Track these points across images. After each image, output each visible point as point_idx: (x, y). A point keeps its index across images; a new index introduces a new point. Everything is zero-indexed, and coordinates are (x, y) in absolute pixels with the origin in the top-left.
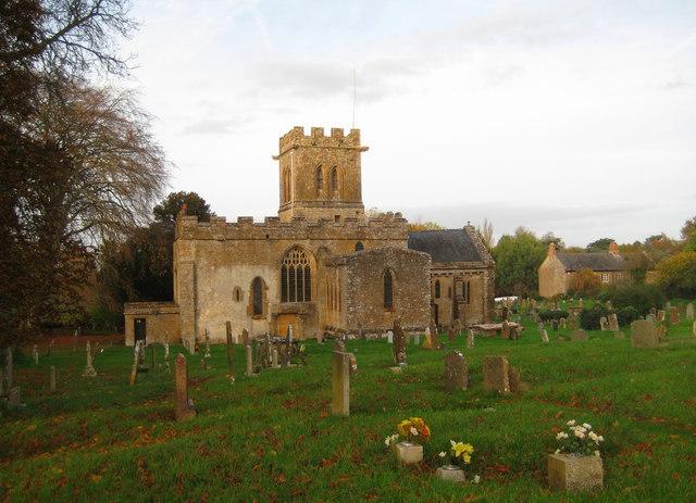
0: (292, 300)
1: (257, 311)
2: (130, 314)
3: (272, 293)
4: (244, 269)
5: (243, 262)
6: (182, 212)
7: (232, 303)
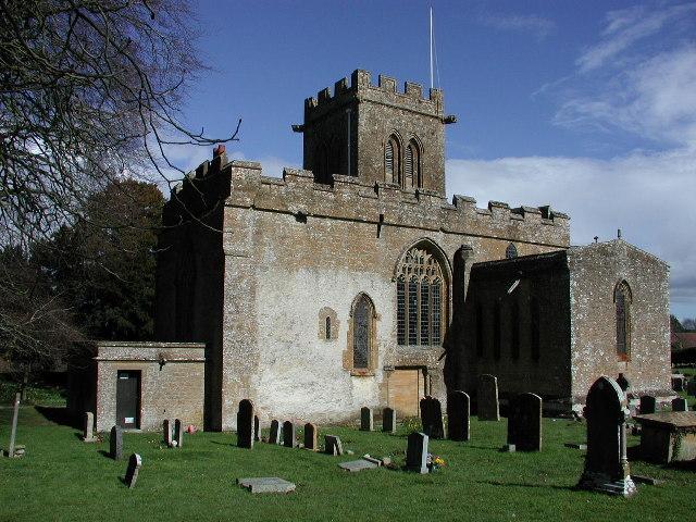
0: (413, 342)
1: (360, 360)
2: (112, 357)
3: (385, 326)
4: (342, 276)
5: (340, 263)
6: (623, 118)
7: (319, 345)
